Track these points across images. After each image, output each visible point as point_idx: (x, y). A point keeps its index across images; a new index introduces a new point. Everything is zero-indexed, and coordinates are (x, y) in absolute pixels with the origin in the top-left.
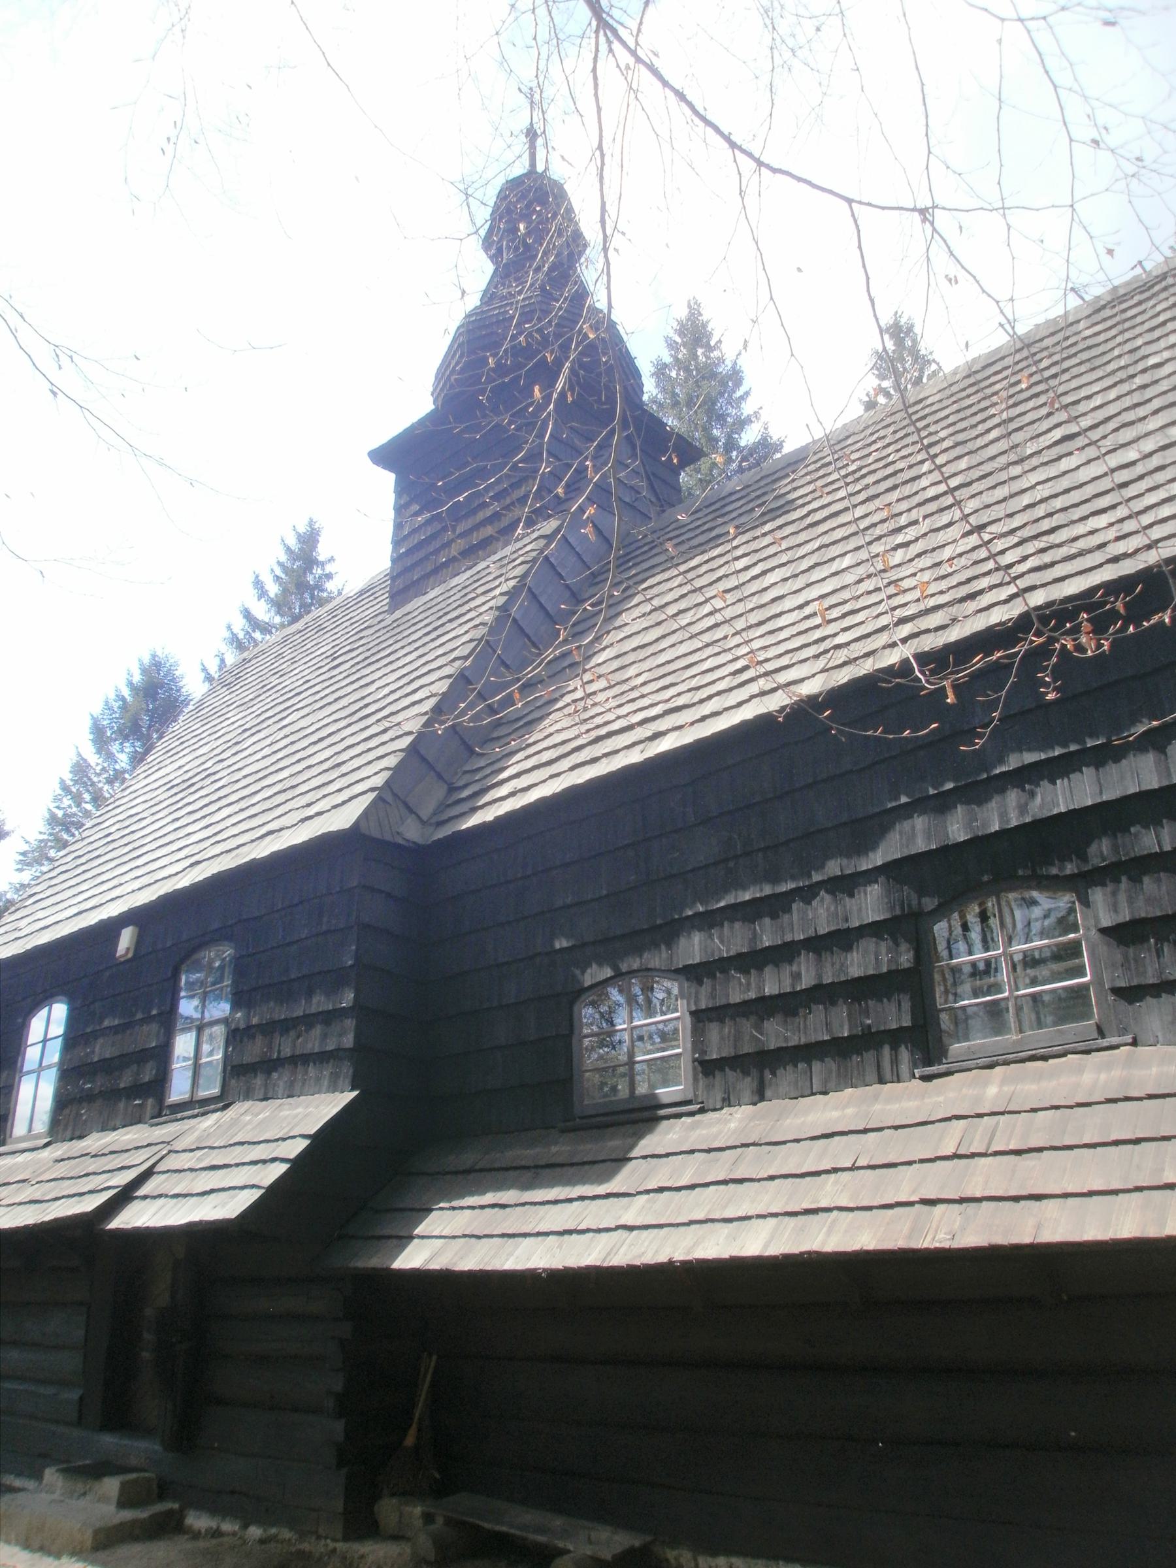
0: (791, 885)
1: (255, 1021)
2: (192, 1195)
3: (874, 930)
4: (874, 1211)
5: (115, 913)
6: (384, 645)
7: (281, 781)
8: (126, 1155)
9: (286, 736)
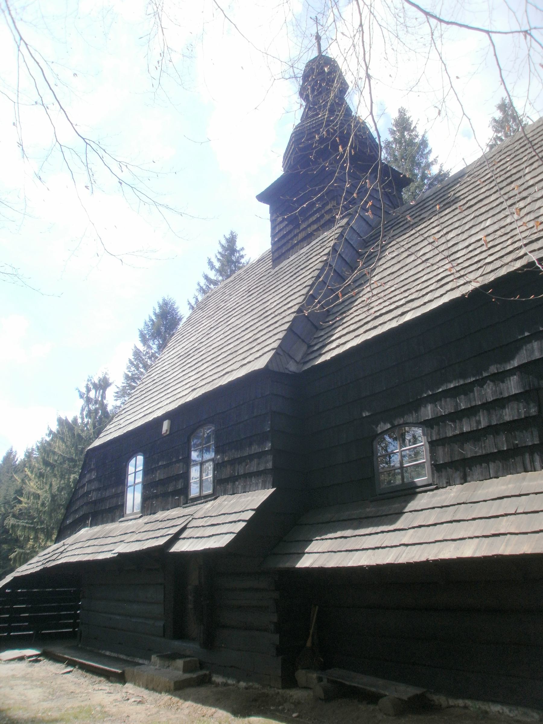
0: (473, 379)
1: (226, 459)
2: (204, 537)
3: (515, 397)
4: (529, 534)
5: (160, 415)
7: (230, 349)
8: (174, 520)
9: (230, 329)
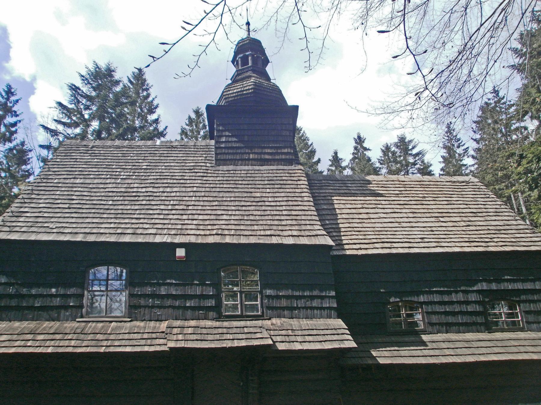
5: (467, 251)
6: (75, 166)
